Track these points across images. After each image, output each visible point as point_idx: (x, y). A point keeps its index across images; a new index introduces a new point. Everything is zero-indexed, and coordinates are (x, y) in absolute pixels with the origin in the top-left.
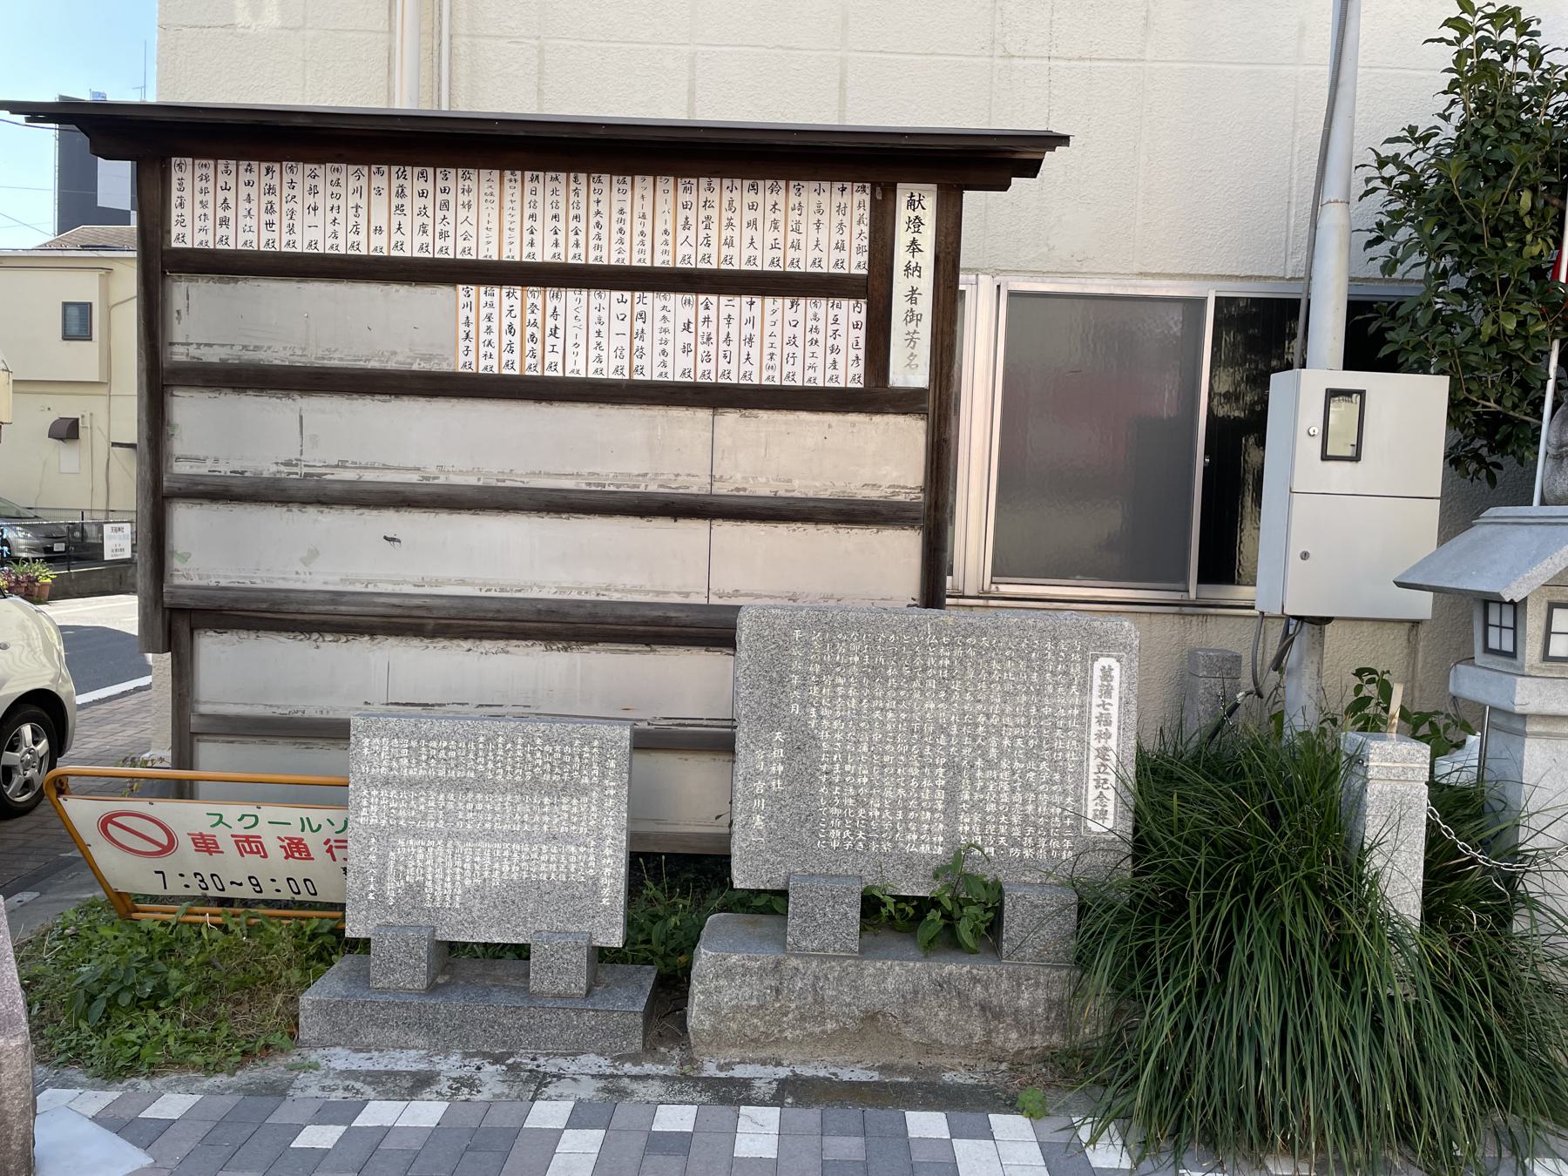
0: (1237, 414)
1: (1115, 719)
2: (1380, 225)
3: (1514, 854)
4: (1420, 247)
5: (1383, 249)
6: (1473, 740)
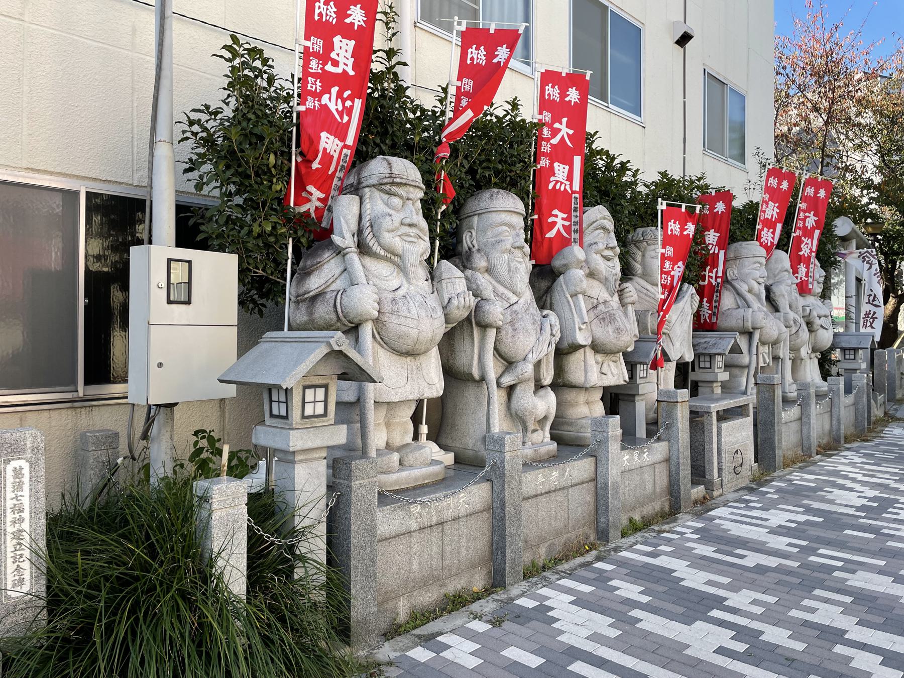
0: (106, 269)
1: (27, 507)
2: (191, 160)
3: (293, 533)
4: (217, 176)
5: (195, 175)
6: (262, 463)
